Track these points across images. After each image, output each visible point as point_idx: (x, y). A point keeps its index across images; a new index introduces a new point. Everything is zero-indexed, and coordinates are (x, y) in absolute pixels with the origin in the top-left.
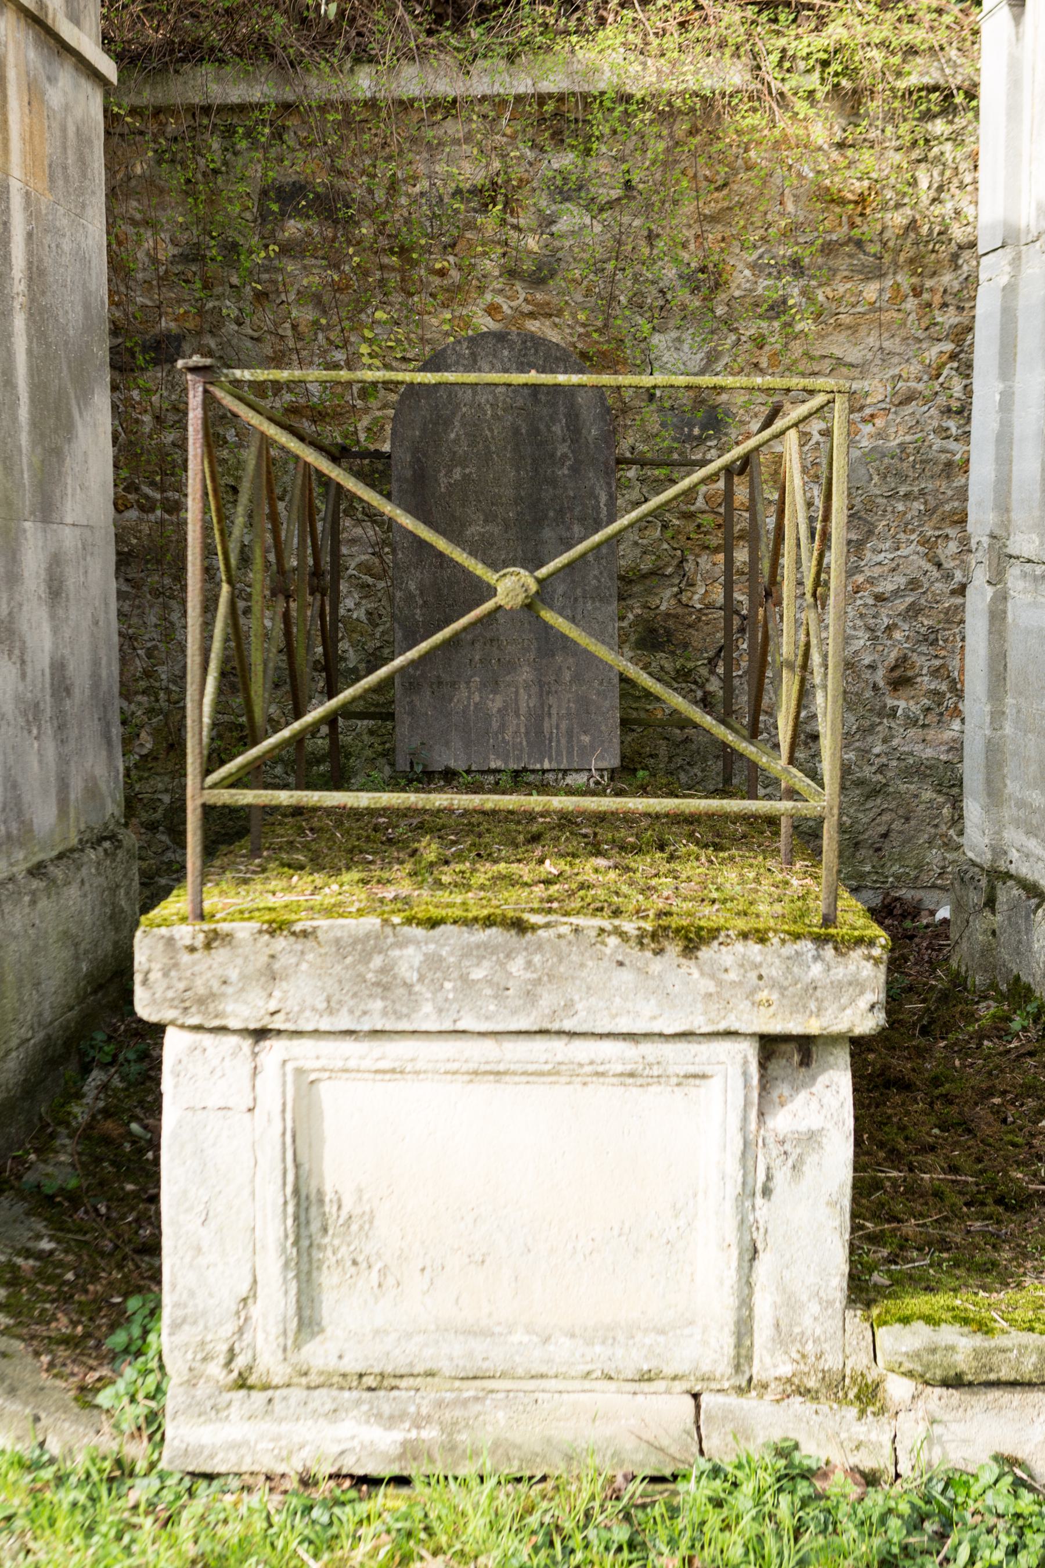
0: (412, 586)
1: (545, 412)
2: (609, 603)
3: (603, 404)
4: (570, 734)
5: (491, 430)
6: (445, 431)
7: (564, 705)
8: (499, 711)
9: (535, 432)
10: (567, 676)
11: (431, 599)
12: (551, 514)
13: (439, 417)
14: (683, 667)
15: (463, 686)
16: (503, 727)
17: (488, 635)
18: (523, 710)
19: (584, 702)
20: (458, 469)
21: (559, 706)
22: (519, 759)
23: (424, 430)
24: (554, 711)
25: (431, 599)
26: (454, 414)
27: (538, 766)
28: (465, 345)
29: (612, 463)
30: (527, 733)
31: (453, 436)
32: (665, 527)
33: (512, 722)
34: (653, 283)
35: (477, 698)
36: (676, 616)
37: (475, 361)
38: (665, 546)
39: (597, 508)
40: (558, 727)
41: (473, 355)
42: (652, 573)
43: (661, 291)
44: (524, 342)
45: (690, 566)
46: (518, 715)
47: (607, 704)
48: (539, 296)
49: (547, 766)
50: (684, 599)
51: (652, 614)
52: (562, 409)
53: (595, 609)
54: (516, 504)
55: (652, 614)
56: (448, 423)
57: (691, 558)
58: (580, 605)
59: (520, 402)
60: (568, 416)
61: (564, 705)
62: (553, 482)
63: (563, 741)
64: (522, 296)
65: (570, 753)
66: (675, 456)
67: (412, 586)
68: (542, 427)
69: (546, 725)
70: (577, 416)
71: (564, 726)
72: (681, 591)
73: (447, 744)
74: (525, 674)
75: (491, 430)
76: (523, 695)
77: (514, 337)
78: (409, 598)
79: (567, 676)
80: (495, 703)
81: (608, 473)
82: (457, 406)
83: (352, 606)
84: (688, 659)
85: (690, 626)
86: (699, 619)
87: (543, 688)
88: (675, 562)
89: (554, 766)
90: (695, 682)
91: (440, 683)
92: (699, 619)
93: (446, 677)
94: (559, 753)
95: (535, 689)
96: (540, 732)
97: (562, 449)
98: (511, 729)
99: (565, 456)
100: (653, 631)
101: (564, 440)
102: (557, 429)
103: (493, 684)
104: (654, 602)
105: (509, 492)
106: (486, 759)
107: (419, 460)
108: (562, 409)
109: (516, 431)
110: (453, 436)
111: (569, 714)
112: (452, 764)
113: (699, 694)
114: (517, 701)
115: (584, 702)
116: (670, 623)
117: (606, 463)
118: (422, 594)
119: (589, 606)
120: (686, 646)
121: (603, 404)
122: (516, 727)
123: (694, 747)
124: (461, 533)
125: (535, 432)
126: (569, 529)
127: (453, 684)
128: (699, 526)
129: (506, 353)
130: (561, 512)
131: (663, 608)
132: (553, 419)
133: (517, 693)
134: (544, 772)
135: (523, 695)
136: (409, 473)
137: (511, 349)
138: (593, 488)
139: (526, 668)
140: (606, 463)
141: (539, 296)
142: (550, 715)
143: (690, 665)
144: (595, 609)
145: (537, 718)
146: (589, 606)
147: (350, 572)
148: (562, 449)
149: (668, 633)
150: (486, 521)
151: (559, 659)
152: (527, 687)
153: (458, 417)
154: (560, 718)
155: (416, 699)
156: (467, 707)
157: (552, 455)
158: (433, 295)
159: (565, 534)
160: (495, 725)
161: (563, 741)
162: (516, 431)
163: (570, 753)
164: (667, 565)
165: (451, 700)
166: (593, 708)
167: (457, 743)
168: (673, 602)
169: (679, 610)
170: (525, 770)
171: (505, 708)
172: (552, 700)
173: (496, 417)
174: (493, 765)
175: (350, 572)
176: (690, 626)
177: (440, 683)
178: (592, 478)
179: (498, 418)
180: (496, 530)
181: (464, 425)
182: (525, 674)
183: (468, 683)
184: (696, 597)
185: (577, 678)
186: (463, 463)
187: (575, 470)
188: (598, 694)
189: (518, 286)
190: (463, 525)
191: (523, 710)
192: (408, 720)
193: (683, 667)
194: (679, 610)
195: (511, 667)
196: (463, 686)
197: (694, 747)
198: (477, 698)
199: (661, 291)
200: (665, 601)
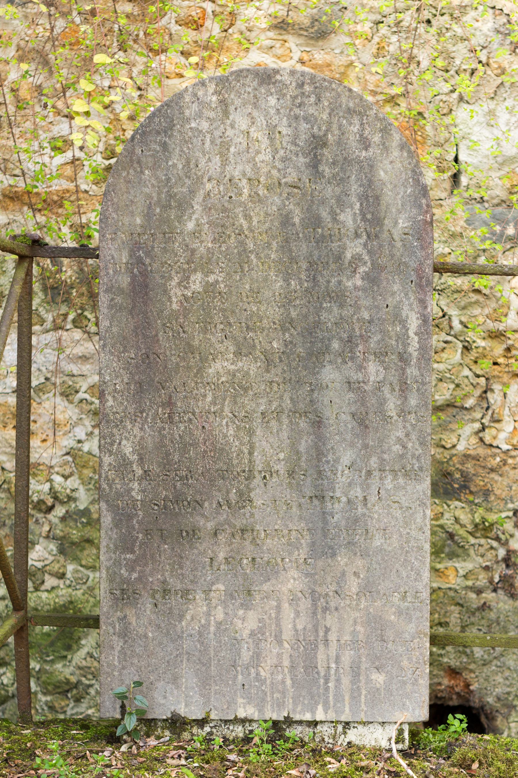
0: (128, 448)
1: (329, 191)
2: (418, 479)
3: (417, 181)
4: (356, 671)
5: (248, 217)
6: (180, 219)
7: (348, 628)
8: (252, 634)
9: (313, 221)
10: (353, 585)
11: (155, 468)
12: (336, 345)
13: (171, 196)
14: (484, 520)
15: (199, 596)
16: (257, 657)
17: (238, 523)
18: (287, 634)
19: (377, 626)
20: (198, 277)
21: (341, 630)
22: (280, 705)
23: (148, 216)
24: (333, 637)
25: (155, 468)
26: (192, 192)
27: (308, 717)
28: (211, 88)
29: (429, 270)
30: (293, 667)
31: (190, 226)
32: (467, 349)
33: (271, 652)
34: (463, 39)
35: (219, 614)
36: (476, 458)
37: (226, 113)
38: (466, 372)
39: (403, 338)
40: (337, 660)
41: (223, 103)
42: (450, 405)
43: (473, 51)
44: (301, 85)
45: (495, 398)
46: (279, 641)
47: (411, 628)
48: (319, 57)
49: (320, 716)
50: (488, 439)
51: (447, 454)
52: (355, 188)
53: (397, 488)
54: (284, 329)
55: (447, 454)
56: (183, 206)
57: (497, 387)
58: (375, 482)
59: (292, 177)
60: (364, 198)
61: (348, 628)
62: (339, 297)
63: (346, 681)
64: (297, 55)
65: (355, 697)
66: (482, 260)
67: (128, 448)
68: (324, 214)
69: (321, 656)
70: (377, 198)
71: (347, 658)
72: (483, 429)
73: (175, 680)
74: (292, 581)
75: (248, 217)
76: (288, 612)
77: (286, 78)
78: (123, 466)
79: (353, 585)
80: (247, 623)
81: (422, 285)
82: (199, 180)
83: (83, 437)
84: (489, 510)
85: (492, 470)
86: (504, 463)
87: (319, 604)
88: (478, 392)
89: (332, 716)
90: (497, 539)
91: (166, 592)
92: (504, 463)
93: (175, 583)
94: (339, 698)
95: (305, 604)
96: (311, 667)
97: (354, 248)
98: (269, 661)
99: (357, 258)
100: (447, 475)
101: (357, 235)
102: (348, 218)
103: (245, 595)
104: (449, 440)
105: (273, 312)
106: (231, 703)
107: (140, 261)
108: (355, 188)
109: (286, 220)
110: (190, 226)
111: (355, 642)
112: (182, 711)
113: (502, 553)
114: (278, 619)
115: (377, 626)
116: (469, 467)
117: (419, 271)
118: (141, 459)
119: (389, 483)
120: (487, 493)
121: (417, 181)
122: (276, 660)
123: (493, 615)
124: (200, 370)
125: (313, 221)
126: (360, 368)
127: (186, 593)
128: (508, 349)
129: (272, 101)
130: (350, 342)
131: (461, 447)
132: (341, 202)
133: (278, 608)
134: (314, 724)
135: (288, 612)
136: (125, 281)
137: (281, 96)
138: (398, 307)
139: (293, 573)
140: (419, 271)
141: (319, 57)
142: (326, 641)
143: (492, 517)
144: (397, 488)
145: (308, 647)
146: (389, 483)
147: (81, 395)
148: (354, 248)
149: (466, 478)
150: (238, 354)
151: (342, 560)
152: (294, 601)
153: (199, 197)
154: (341, 647)
155: (130, 613)
156: (206, 627)
157: (339, 258)
158: (185, 54)
159: (356, 376)
160: (246, 655)
161: (346, 681)
162: (286, 220)
163: (355, 697)
164: (466, 396)
165: (181, 617)
166: (390, 634)
167: (189, 678)
168: (474, 440)
169: (481, 451)
170: (289, 721)
171: (261, 630)
172: (330, 620)
173: (256, 198)
174: (241, 714)
175: (81, 395)
176: (492, 470)
177: (166, 592)
178: (397, 291)
179: (256, 198)
180: (251, 367)
181: (207, 209)
182: (292, 581)
183: (207, 592)
184: (502, 436)
185: (368, 589)
186: (206, 266)
187: (372, 280)
188: (399, 613)
189: (292, 41)
190: (204, 360)
191: (287, 634)
192: (118, 644)
193: (484, 520)
194: (481, 451)
195: (271, 570)
196: (199, 596)
197: (493, 615)
198: (219, 614)
199: (473, 51)
200: (463, 439)
